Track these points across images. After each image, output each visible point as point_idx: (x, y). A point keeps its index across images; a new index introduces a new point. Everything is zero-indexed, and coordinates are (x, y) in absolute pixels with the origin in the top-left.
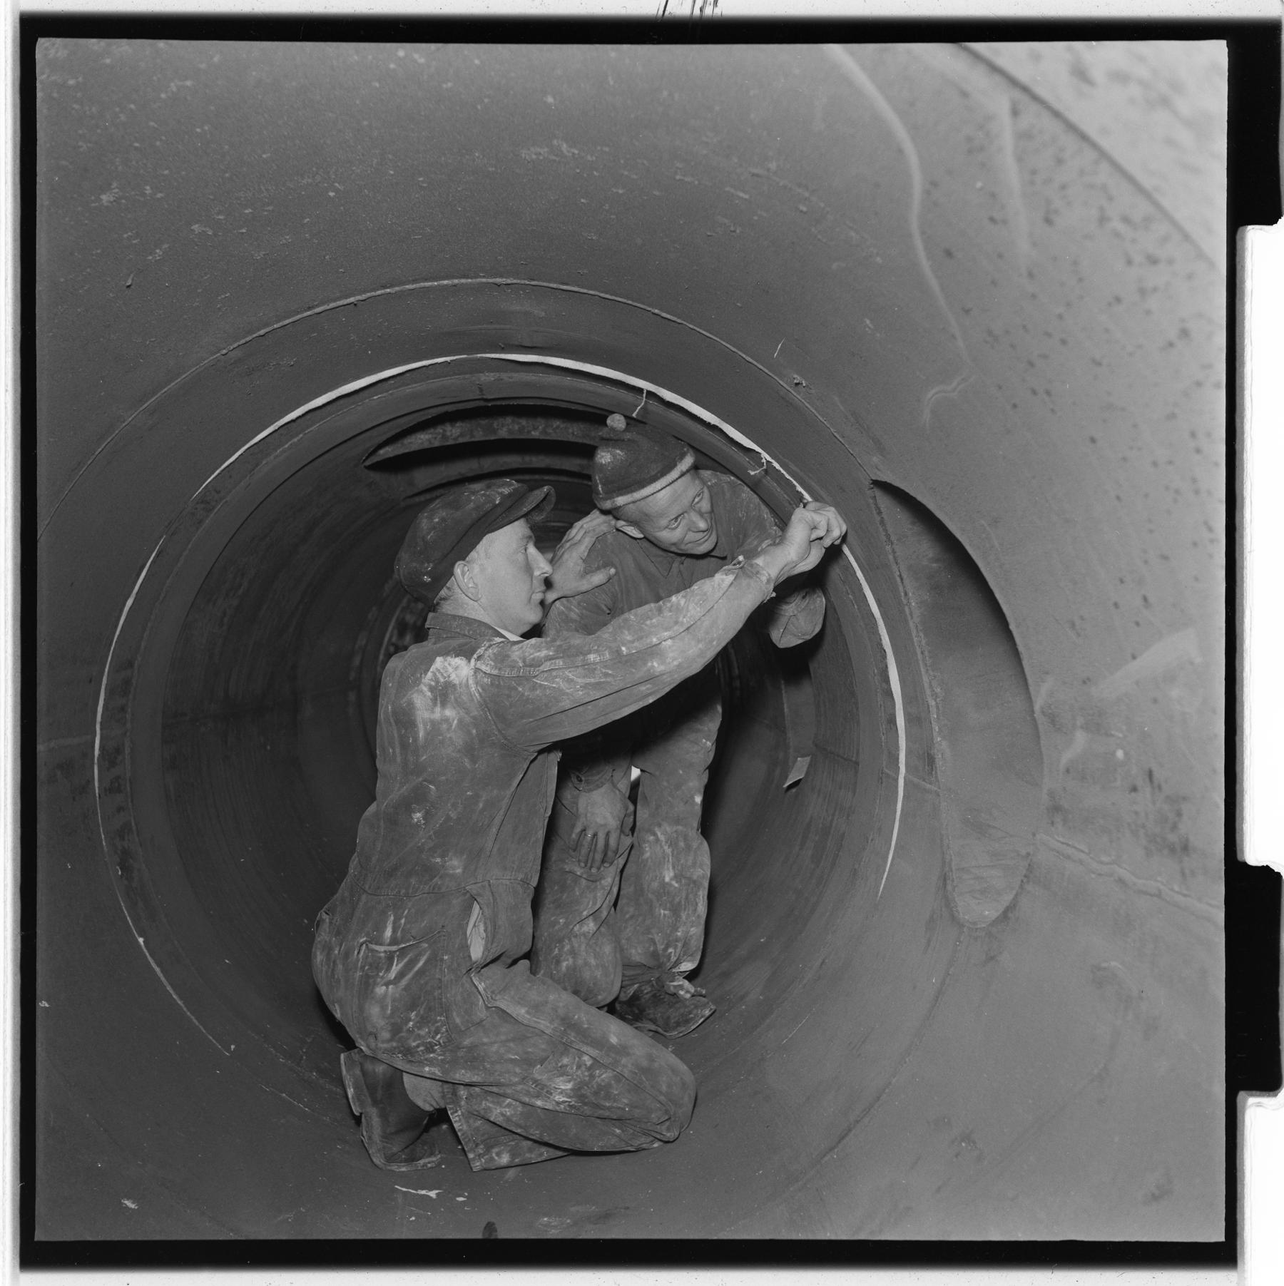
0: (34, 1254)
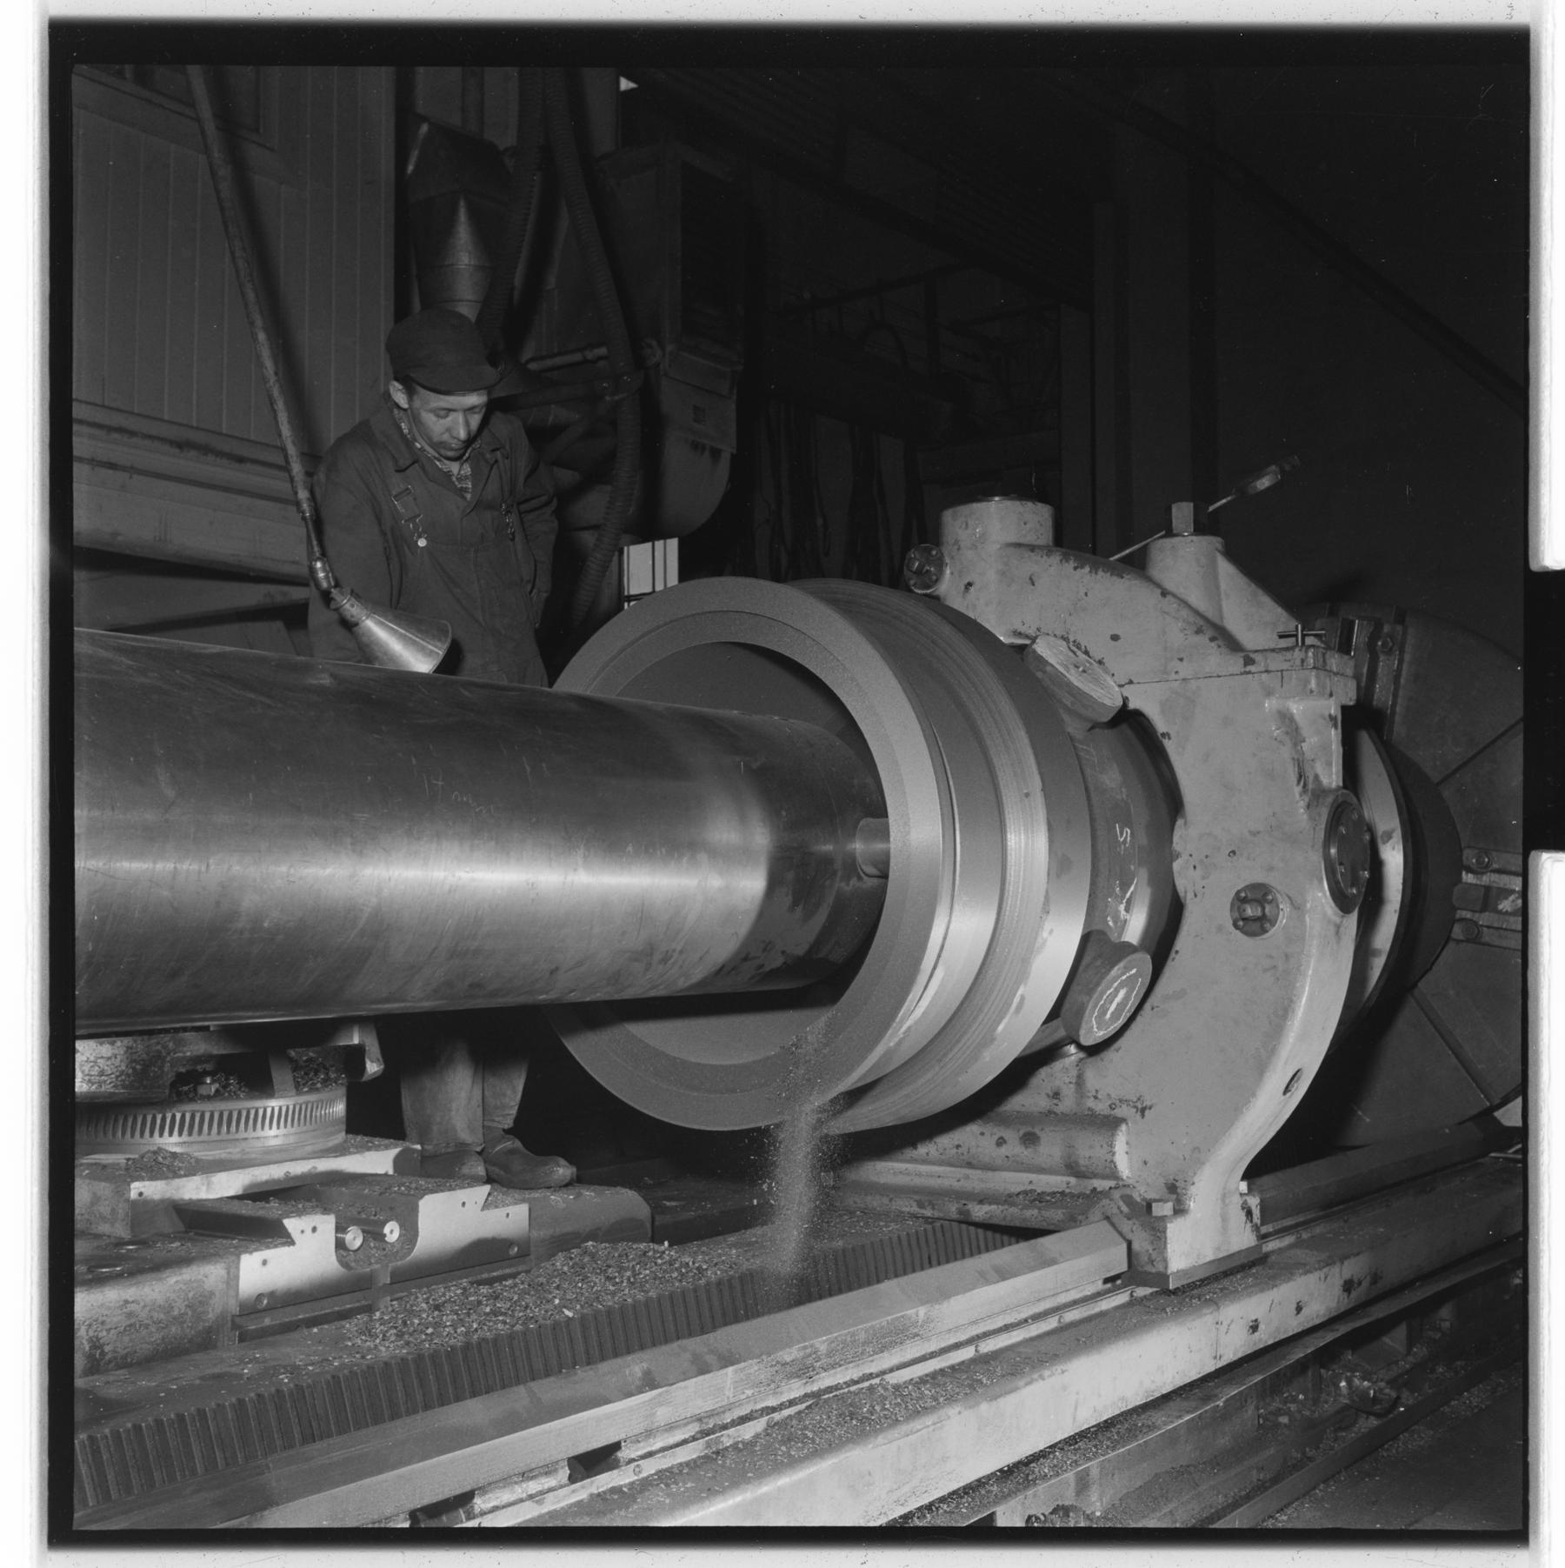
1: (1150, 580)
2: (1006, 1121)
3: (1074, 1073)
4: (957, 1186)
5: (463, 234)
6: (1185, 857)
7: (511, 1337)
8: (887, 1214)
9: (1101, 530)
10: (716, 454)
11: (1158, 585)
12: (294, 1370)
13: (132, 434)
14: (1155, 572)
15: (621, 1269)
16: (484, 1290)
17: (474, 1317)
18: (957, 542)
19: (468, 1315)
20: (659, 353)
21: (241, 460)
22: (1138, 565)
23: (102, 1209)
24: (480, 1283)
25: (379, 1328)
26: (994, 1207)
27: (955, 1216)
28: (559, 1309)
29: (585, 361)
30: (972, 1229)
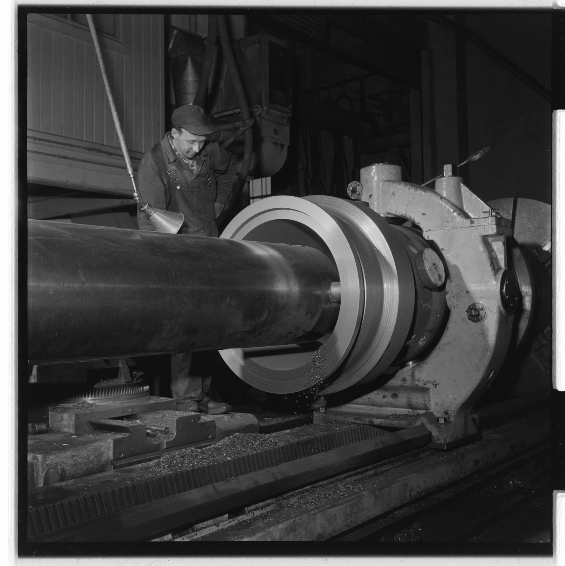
0: (26, 547)
1: (436, 193)
2: (386, 390)
3: (411, 372)
4: (369, 412)
5: (190, 69)
6: (450, 293)
7: (209, 467)
8: (344, 422)
9: (418, 174)
10: (282, 146)
11: (439, 195)
12: (132, 479)
13: (73, 146)
14: (437, 190)
15: (248, 443)
16: (199, 450)
17: (195, 460)
18: (366, 180)
19: (194, 459)
20: (261, 110)
21: (111, 154)
22: (432, 187)
23: (65, 423)
24: (197, 448)
25: (162, 465)
26: (382, 420)
27: (368, 423)
28: (225, 457)
29: (234, 114)
30: (374, 428)
